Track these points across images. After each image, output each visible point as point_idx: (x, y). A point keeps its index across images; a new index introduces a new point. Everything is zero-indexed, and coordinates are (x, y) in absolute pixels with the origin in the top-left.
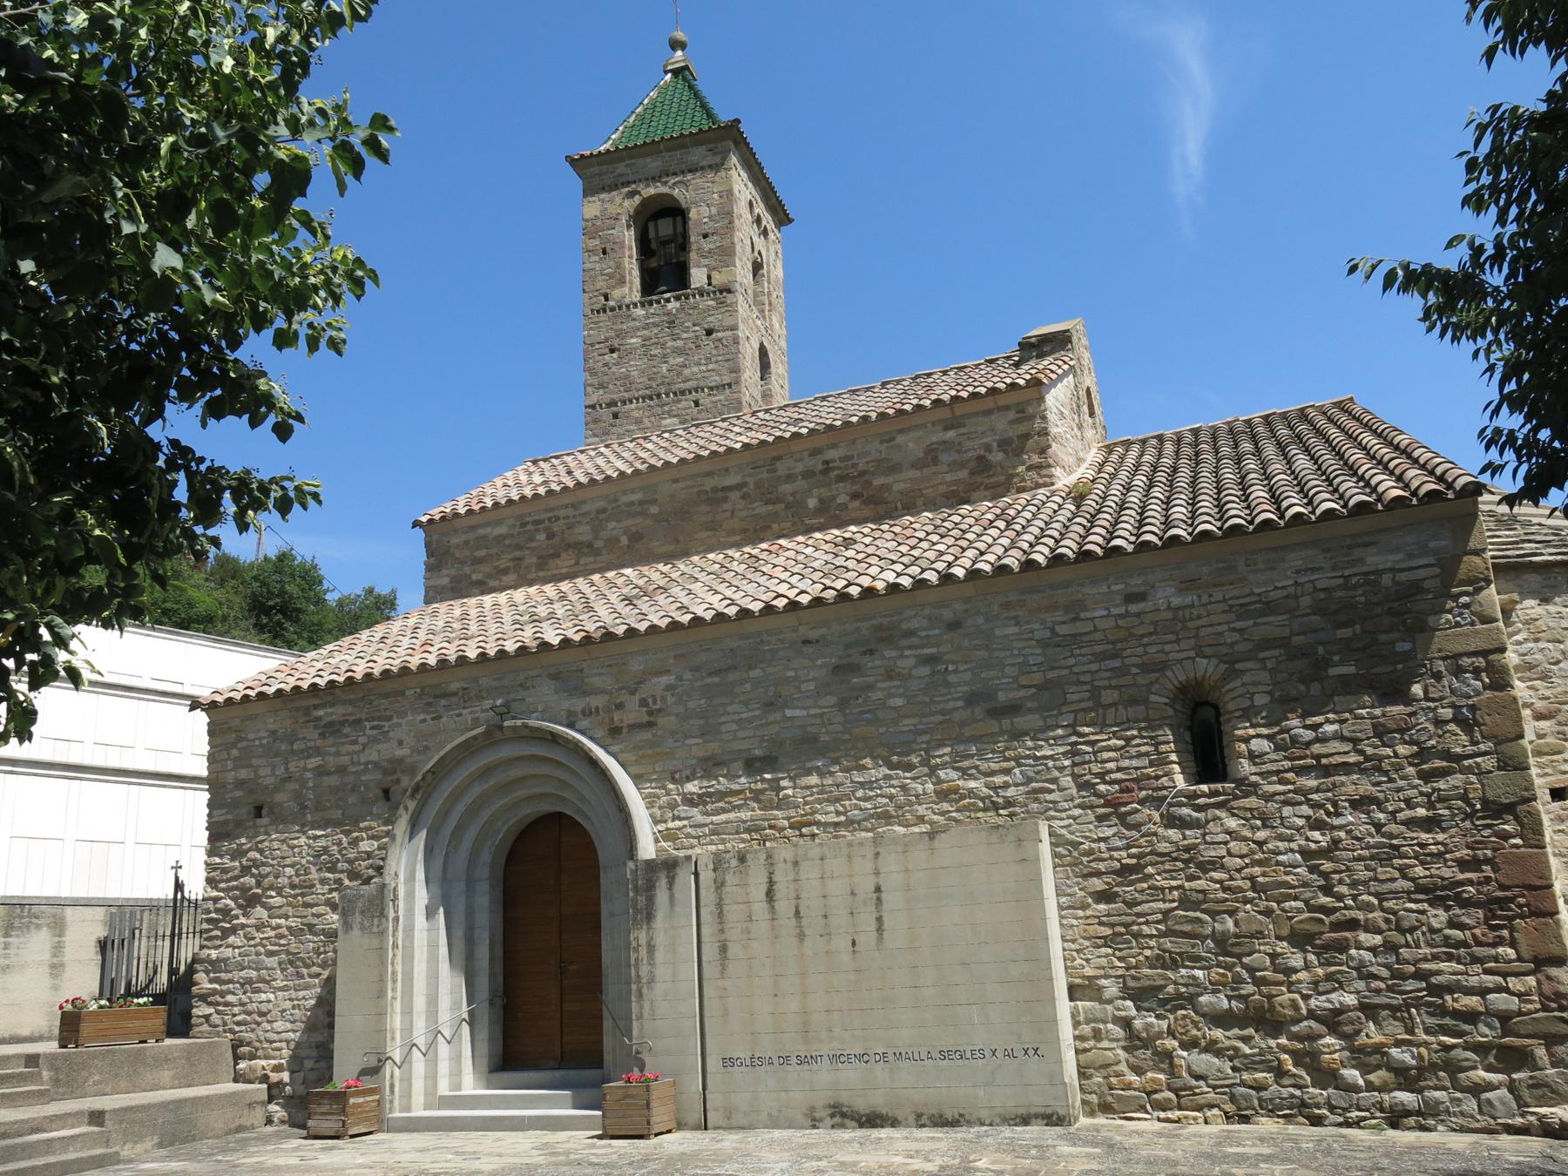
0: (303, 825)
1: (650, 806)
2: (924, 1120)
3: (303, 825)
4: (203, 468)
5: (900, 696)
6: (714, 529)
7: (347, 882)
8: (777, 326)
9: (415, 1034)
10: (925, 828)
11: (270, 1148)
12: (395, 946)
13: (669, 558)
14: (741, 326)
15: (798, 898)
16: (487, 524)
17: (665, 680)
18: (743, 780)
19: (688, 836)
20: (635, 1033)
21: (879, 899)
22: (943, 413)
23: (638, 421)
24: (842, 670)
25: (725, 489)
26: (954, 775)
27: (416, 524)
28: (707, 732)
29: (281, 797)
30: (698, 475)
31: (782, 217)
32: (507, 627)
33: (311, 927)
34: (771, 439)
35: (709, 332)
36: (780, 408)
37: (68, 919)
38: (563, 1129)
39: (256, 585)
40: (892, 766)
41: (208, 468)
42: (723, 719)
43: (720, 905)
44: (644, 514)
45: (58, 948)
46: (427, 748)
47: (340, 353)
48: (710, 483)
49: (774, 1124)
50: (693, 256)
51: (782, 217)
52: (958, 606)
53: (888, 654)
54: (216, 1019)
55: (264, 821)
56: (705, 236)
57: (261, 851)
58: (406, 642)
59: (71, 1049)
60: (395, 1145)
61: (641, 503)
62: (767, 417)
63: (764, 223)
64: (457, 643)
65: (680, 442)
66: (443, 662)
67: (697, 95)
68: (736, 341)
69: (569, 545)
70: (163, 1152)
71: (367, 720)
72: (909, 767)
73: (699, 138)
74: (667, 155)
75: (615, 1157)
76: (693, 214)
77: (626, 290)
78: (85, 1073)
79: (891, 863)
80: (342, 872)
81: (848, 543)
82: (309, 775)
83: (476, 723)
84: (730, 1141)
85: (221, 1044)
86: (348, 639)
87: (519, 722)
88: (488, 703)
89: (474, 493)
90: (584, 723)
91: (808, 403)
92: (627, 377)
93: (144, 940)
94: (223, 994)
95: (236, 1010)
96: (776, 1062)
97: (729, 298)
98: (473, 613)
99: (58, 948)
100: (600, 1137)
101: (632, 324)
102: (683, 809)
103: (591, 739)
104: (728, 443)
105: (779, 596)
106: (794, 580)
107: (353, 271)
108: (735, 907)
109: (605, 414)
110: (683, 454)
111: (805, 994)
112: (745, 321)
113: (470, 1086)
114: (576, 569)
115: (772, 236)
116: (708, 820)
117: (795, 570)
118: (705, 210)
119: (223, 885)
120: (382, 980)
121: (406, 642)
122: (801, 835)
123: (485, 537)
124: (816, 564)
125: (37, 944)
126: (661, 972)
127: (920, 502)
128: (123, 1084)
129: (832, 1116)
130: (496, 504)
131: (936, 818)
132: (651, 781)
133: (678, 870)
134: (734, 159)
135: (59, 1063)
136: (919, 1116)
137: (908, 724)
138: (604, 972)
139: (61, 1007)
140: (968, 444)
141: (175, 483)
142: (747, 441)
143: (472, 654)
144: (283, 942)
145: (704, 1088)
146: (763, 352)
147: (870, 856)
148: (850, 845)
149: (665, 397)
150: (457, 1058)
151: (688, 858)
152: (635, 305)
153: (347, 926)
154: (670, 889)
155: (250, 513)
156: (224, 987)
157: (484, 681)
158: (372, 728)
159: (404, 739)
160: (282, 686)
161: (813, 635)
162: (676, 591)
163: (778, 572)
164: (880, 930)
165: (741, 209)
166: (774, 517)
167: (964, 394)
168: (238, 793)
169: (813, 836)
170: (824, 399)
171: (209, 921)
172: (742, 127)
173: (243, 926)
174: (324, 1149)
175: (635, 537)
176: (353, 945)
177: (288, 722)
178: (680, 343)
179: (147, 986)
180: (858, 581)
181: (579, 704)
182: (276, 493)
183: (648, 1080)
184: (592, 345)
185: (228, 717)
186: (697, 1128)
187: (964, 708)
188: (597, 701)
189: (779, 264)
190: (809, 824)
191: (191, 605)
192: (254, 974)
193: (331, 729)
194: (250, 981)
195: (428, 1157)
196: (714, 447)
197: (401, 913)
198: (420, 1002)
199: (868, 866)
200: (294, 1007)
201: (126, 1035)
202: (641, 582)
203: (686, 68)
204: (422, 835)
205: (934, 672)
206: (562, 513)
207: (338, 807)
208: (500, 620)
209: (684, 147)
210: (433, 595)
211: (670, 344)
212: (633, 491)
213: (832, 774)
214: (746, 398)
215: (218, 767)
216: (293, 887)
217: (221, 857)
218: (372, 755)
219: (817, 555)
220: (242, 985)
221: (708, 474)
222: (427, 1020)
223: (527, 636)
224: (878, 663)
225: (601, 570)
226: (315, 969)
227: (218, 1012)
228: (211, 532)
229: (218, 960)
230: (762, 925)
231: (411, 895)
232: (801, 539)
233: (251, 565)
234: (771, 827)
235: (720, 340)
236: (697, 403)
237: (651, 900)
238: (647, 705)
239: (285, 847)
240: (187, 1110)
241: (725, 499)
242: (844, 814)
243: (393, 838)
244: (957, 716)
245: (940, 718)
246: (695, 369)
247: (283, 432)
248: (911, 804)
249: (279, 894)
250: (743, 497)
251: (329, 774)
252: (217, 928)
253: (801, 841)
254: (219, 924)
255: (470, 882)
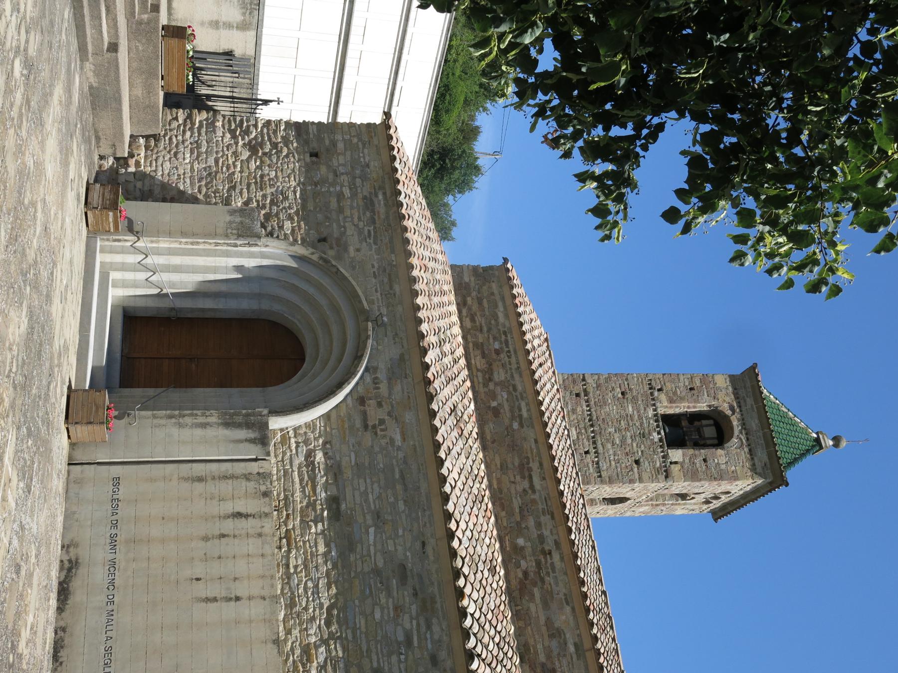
0: (304, 184)
1: (307, 425)
2: (60, 633)
3: (304, 184)
4: (638, 149)
5: (382, 616)
6: (502, 469)
7: (263, 212)
8: (641, 510)
9: (154, 257)
10: (282, 635)
11: (83, 159)
12: (217, 244)
13: (481, 436)
14: (642, 485)
15: (235, 536)
16: (505, 307)
17: (398, 438)
18: (323, 495)
19: (284, 453)
20: (143, 413)
21: (231, 599)
22: (587, 644)
23: (574, 411)
24: (403, 572)
25: (530, 477)
26: (321, 659)
27: (506, 260)
28: (359, 467)
29: (323, 169)
30: (540, 458)
31: (718, 514)
32: (437, 324)
33: (234, 188)
34: (567, 512)
35: (637, 462)
36: (586, 516)
37: (248, 33)
38: (78, 360)
39: (460, 151)
40: (329, 609)
41: (638, 154)
42: (368, 481)
43: (233, 477)
44: (513, 418)
45: (229, 26)
46: (354, 268)
47: (732, 260)
48: (534, 466)
49: (68, 516)
50: (691, 451)
51: (718, 514)
52: (448, 664)
53: (414, 607)
54: (175, 124)
55: (308, 159)
56: (705, 460)
57: (287, 156)
58: (427, 254)
59: (161, 32)
60: (77, 242)
61: (521, 416)
62: (581, 506)
63: (714, 502)
64: (426, 289)
65: (563, 442)
66: (414, 280)
67: (803, 455)
68: (631, 481)
69: (491, 365)
70: (86, 89)
71: (375, 228)
72: (328, 623)
73: (773, 457)
74: (760, 434)
75: (53, 400)
76: (720, 452)
77: (666, 404)
78: (144, 41)
79: (257, 609)
80: (270, 209)
81: (493, 571)
82: (338, 188)
83: (371, 302)
84: (58, 484)
85: (157, 128)
86: (427, 213)
87: (370, 333)
88: (384, 311)
89: (526, 299)
90: (368, 379)
91: (590, 536)
92: (605, 403)
93: (231, 80)
94: (191, 129)
95: (180, 138)
96: (114, 518)
97: (662, 477)
98: (445, 299)
99: (229, 26)
100: (70, 387)
101: (642, 407)
102: (304, 449)
103: (357, 384)
104: (563, 479)
105: (458, 523)
106: (468, 533)
107: (827, 284)
108: (230, 488)
109: (579, 388)
110: (555, 447)
111: (163, 541)
112: (645, 488)
113: (115, 294)
114: (475, 370)
115: (705, 507)
116: (295, 469)
117: (474, 532)
118: (723, 460)
119: (265, 130)
120: (194, 235)
121: (427, 254)
122: (281, 539)
123: (496, 306)
124: (478, 547)
125: (234, 14)
126: (186, 433)
127: (521, 624)
128: (135, 65)
129: (70, 561)
130: (519, 315)
131: (289, 644)
132: (325, 426)
133: (260, 446)
134: (760, 481)
135: (152, 25)
136: (64, 630)
137: (361, 622)
138: (189, 390)
139: (189, 27)
140: (564, 662)
141: (624, 126)
142: (565, 494)
143: (420, 301)
144: (224, 169)
145: (99, 463)
146: (623, 500)
147: (263, 593)
148: (272, 577)
149: (591, 428)
150: (135, 285)
151: (268, 454)
152: (655, 410)
153: (233, 212)
154: (246, 440)
155: (595, 184)
156: (196, 130)
157: (400, 309)
158: (369, 231)
159: (360, 251)
160: (400, 172)
161: (429, 550)
162: (460, 443)
163: (473, 519)
164: (207, 600)
165: (725, 486)
166: (510, 514)
167: (601, 660)
168: (327, 142)
169: (280, 548)
170: (593, 547)
171: (242, 121)
172: (782, 488)
173: (237, 143)
174: (78, 195)
175: (496, 412)
176: (220, 216)
177: (374, 175)
178: (629, 441)
179: (200, 81)
180: (468, 584)
181: (382, 375)
182: (612, 206)
183: (108, 422)
184: (627, 379)
185: (380, 135)
186: (70, 457)
187: (372, 667)
188: (384, 388)
189: (685, 512)
190: (289, 544)
191: (447, 111)
192: (204, 149)
193: (369, 203)
194: (199, 147)
195: (66, 266)
196: (560, 469)
197: (240, 249)
198: (176, 260)
199: (256, 592)
200: (179, 175)
201: (168, 68)
202: (465, 417)
203: (821, 448)
204: (294, 264)
205: (399, 643)
206: (513, 360)
207: (315, 208)
208: (441, 319)
209: (767, 446)
210: (457, 271)
211: (629, 434)
212: (528, 410)
213: (326, 563)
214: (591, 488)
215: (346, 129)
216: (262, 176)
217: (285, 130)
218: (350, 231)
219: (485, 547)
220: (196, 142)
221: (541, 464)
222: (163, 265)
223: (432, 339)
224: (407, 599)
225: (473, 387)
226: (204, 190)
227: (179, 126)
228: (576, 152)
229: (215, 127)
230: (217, 508)
231: (252, 255)
232: (495, 532)
233: (472, 149)
234: (288, 515)
235: (632, 470)
236: (587, 453)
237: (239, 426)
238: (380, 424)
239: (289, 171)
240: (113, 105)
241: (523, 477)
242: (295, 572)
243: (292, 244)
244: (366, 662)
245: (364, 648)
246: (611, 452)
247: (671, 215)
248: (301, 624)
249: (257, 167)
250: (524, 490)
251: (338, 201)
252: (236, 127)
253: (276, 538)
254: (239, 128)
255: (259, 296)
